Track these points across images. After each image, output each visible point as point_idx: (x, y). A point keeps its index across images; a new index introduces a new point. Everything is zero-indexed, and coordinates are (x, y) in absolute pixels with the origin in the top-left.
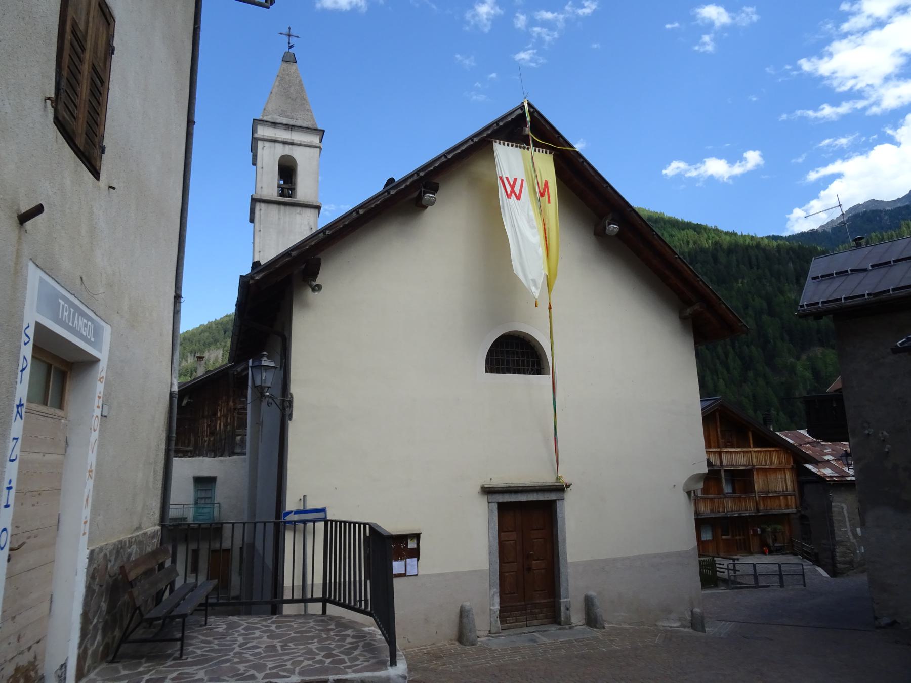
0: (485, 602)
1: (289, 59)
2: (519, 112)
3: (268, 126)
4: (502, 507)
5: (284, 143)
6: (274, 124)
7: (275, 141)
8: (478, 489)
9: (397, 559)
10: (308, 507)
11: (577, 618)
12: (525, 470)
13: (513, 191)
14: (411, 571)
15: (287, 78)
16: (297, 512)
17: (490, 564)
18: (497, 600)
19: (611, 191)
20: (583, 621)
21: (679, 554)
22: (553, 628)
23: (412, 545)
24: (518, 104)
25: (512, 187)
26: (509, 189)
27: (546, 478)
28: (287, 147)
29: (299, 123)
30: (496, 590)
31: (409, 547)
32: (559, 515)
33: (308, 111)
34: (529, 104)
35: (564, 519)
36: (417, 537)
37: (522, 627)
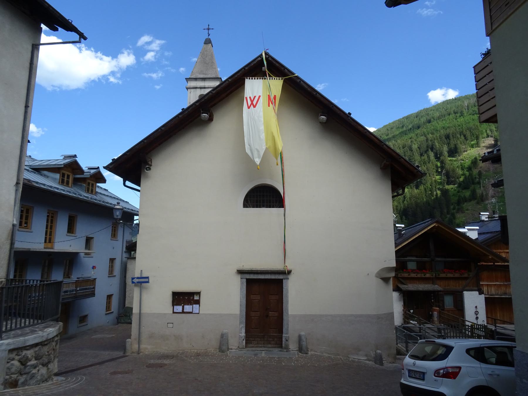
0: (237, 331)
1: (208, 42)
2: (259, 59)
3: (199, 81)
4: (249, 281)
5: (201, 88)
6: (196, 79)
7: (196, 88)
8: (236, 271)
9: (188, 305)
10: (144, 276)
11: (293, 346)
12: (266, 260)
13: (252, 103)
14: (196, 310)
15: (205, 53)
16: (138, 278)
17: (241, 311)
18: (244, 331)
19: (320, 96)
20: (297, 349)
21: (369, 316)
22: (276, 350)
23: (196, 298)
24: (259, 54)
25: (252, 101)
26: (249, 103)
27: (278, 266)
28: (202, 90)
29: (209, 76)
30: (243, 325)
31: (195, 298)
32: (21, 250)
33: (214, 68)
34: (266, 54)
35: (287, 290)
36: (199, 294)
37: (261, 347)
